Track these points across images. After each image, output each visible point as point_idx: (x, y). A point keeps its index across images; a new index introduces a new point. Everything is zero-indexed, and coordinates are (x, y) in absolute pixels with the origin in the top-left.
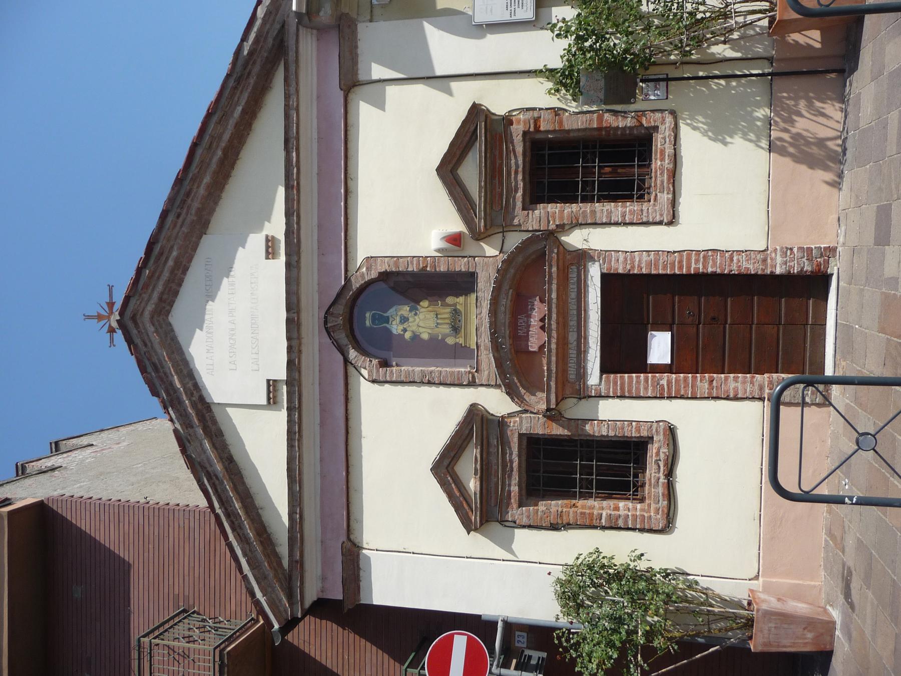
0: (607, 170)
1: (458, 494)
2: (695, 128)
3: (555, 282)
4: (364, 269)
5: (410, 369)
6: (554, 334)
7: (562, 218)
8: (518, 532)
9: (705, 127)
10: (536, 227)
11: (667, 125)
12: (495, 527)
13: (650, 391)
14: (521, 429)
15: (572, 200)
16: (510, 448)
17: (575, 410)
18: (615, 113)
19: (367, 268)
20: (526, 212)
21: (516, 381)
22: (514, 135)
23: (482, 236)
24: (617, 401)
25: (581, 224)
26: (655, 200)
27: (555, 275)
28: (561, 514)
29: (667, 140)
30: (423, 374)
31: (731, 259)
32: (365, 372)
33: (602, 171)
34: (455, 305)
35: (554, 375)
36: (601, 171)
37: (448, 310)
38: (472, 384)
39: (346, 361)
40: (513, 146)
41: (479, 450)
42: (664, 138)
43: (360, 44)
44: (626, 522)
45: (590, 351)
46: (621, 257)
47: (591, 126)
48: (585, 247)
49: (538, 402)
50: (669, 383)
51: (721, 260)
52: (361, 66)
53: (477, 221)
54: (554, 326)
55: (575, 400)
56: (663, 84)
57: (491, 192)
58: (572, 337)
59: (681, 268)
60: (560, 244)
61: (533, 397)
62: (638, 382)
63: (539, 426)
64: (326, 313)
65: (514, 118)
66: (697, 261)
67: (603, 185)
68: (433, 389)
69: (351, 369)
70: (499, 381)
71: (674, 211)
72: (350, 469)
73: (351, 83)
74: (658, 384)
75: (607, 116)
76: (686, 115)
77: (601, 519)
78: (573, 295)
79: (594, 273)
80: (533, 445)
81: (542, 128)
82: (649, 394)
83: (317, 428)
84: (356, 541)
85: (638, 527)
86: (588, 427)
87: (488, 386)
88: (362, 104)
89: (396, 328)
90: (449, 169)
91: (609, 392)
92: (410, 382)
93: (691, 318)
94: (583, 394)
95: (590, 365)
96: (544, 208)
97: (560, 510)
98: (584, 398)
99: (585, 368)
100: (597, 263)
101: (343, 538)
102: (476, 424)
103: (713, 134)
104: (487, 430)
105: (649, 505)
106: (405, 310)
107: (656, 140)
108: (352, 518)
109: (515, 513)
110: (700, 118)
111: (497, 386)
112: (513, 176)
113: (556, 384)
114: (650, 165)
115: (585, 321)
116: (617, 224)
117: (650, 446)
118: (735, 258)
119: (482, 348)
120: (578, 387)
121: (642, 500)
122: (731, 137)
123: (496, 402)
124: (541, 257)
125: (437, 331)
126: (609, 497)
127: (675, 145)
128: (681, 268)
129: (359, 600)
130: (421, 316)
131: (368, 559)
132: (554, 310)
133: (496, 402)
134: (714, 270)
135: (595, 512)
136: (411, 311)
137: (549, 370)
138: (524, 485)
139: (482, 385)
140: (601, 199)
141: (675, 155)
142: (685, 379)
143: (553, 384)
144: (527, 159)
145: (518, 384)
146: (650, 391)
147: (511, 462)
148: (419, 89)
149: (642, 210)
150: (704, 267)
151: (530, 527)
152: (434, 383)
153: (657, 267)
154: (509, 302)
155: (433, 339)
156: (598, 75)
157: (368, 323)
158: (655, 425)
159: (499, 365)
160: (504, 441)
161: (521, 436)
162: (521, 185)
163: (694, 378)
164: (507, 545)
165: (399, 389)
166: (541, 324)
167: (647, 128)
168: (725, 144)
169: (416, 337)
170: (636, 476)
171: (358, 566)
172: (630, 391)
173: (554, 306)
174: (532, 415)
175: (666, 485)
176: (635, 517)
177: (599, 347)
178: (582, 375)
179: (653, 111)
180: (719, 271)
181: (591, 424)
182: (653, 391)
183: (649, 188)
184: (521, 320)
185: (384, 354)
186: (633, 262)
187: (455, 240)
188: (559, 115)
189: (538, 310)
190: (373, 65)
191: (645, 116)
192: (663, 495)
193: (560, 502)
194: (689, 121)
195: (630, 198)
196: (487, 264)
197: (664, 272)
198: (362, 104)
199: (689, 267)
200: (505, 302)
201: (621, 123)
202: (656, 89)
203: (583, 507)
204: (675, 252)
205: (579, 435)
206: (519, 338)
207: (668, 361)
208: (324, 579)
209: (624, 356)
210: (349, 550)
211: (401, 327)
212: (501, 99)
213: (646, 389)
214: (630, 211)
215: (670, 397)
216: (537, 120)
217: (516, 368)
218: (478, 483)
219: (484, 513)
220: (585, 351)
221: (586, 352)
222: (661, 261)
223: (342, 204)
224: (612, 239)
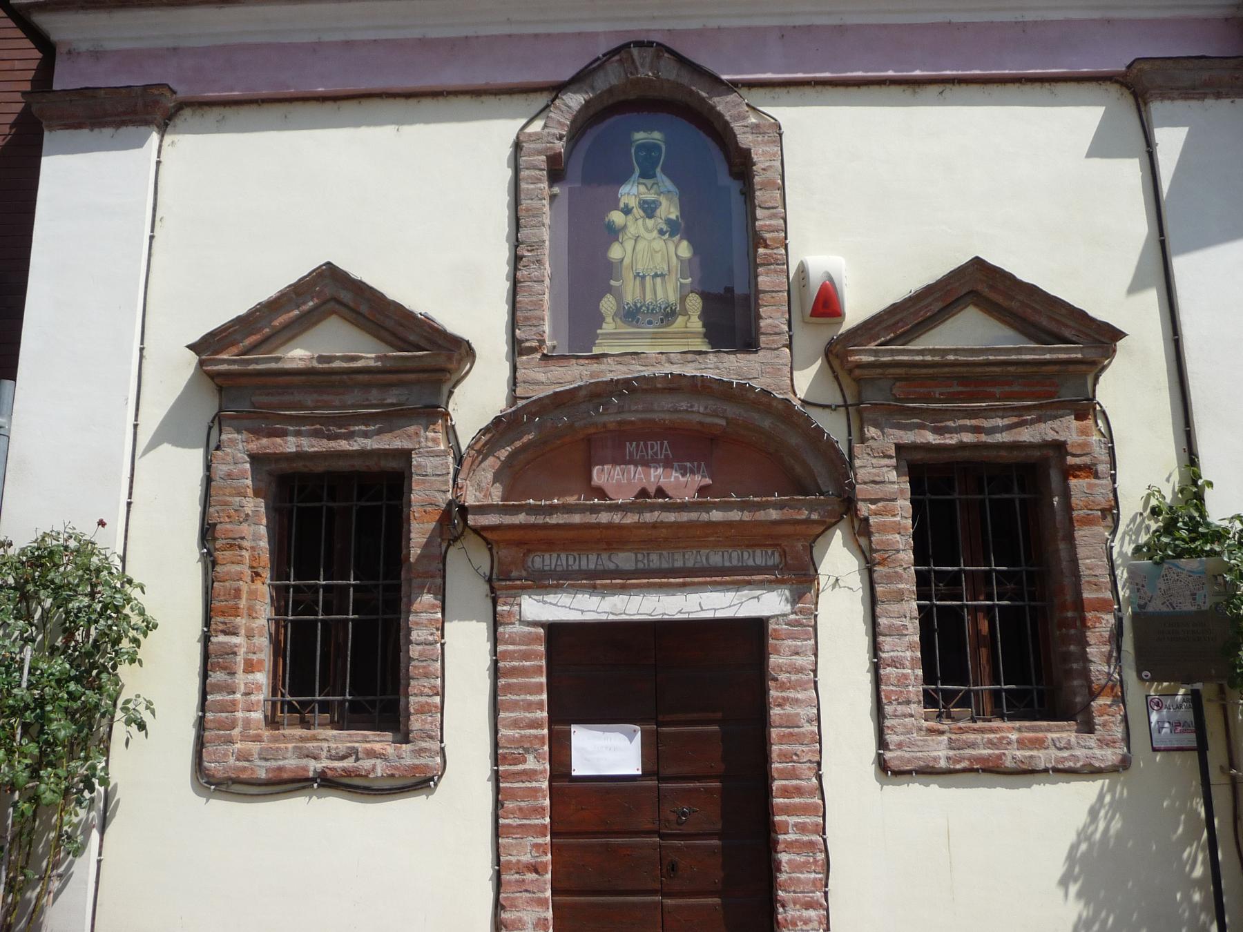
0: (984, 626)
1: (276, 323)
2: (1093, 813)
3: (747, 516)
4: (753, 120)
5: (547, 221)
6: (631, 519)
7: (884, 529)
8: (196, 457)
9: (1098, 836)
10: (862, 474)
11: (1098, 752)
12: (208, 406)
13: (510, 732)
14: (421, 455)
15: (920, 556)
16: (379, 432)
17: (466, 570)
18: (1117, 635)
19: (757, 126)
20: (892, 452)
21: (525, 439)
22: (1056, 424)
23: (836, 363)
24: (486, 661)
25: (870, 572)
26: (931, 731)
27: (761, 515)
28: (235, 545)
29: (1065, 754)
30: (535, 246)
31: (809, 905)
32: (537, 126)
33: (980, 615)
34: (685, 312)
35: (540, 520)
36: (979, 611)
37: (673, 297)
38: (517, 348)
39: (558, 89)
40: (1032, 422)
41: (372, 363)
42: (1068, 747)
43: (1225, 103)
44: (219, 688)
45: (595, 600)
46: (804, 661)
47: (1084, 586)
48: (823, 580)
49: (480, 488)
50: (530, 775)
51: (807, 882)
52: (1180, 106)
53: (872, 346)
54: (649, 517)
55: (486, 569)
56: (1190, 739)
57: (933, 378)
58: (624, 559)
59: (786, 792)
60: (827, 527)
61: (490, 476)
62: (529, 706)
63: (427, 494)
64: (658, 44)
65: (1090, 422)
66: (802, 828)
67: (952, 618)
68: (504, 269)
69: (541, 100)
70: (521, 403)
71: (909, 772)
72: (329, 106)
73: (1141, 88)
74: (527, 750)
75: (1109, 619)
76: (1122, 791)
77: (225, 633)
78: (716, 559)
79: (767, 603)
80: (387, 484)
81: (1073, 482)
82: (503, 732)
83: (416, 33)
84: (178, 121)
85: (209, 715)
86: (427, 599)
87: (514, 382)
88: (1099, 111)
89: (631, 193)
90: (978, 285)
91: (506, 643)
92: (517, 220)
93: (673, 817)
94: (500, 585)
95: (564, 599)
96: (902, 491)
97: (245, 544)
98: (492, 589)
99: (557, 588)
100: (788, 608)
101: (183, 92)
102: (429, 357)
103: (1083, 854)
104: (418, 382)
105: (257, 739)
106: (669, 210)
107: (1062, 730)
108: (227, 111)
109: (239, 448)
110: (1116, 825)
111: (513, 398)
112: (968, 422)
113: (521, 527)
114: (1002, 717)
115: (661, 586)
116: (875, 648)
117: (389, 735)
118: (812, 913)
119: (595, 367)
120: (514, 574)
121: (272, 722)
122: (1079, 895)
123: (478, 399)
124: (800, 486)
125: (628, 276)
126: (278, 651)
127: (1056, 770)
128: (786, 792)
129: (51, 128)
130: (658, 244)
131: (140, 143)
132: (685, 517)
133: (478, 399)
134: (785, 867)
135: (241, 621)
136: (669, 222)
137: (553, 509)
138: (299, 466)
139: (514, 369)
140: (925, 615)
141: (1033, 772)
142: (538, 811)
143: (521, 518)
144: (1003, 453)
145: (518, 444)
146: (510, 732)
147: (349, 436)
148: (1139, 227)
149: (908, 702)
150: (790, 845)
151: (208, 480)
152: (516, 269)
153: (784, 739)
154: (698, 418)
155: (611, 269)
156: (1206, 601)
157: (640, 136)
158: (435, 746)
159: (560, 401)
160: (392, 418)
161: (406, 455)
162: (951, 440)
163: (540, 830)
164: (170, 432)
165: (502, 199)
166: (652, 490)
167: (1087, 708)
168: (1064, 882)
169: (614, 233)
170: (325, 707)
171: (123, 123)
172: (509, 688)
173: (693, 516)
174: (451, 476)
175: (301, 774)
176: (231, 707)
177: (604, 617)
178: (542, 583)
179: (1125, 719)
180: (782, 877)
181: (434, 606)
182: (511, 740)
183: (949, 716)
184: (659, 448)
185: (575, 169)
186: (793, 686)
187: (827, 304)
188: (1104, 517)
189: (682, 483)
190: (1186, 129)
191: (1114, 703)
192: (280, 769)
193: (264, 544)
194: (1108, 799)
195: (929, 678)
196: (777, 372)
197: (774, 756)
198: (1099, 111)
199: (788, 810)
200: (698, 411)
201: (1096, 651)
202: (1175, 726)
203: (253, 595)
204: (819, 778)
205: (410, 581)
206: (621, 443)
207: (578, 769)
208: (97, 55)
209: (589, 673)
210: (156, 102)
211: (633, 202)
212: (1129, 393)
213: (516, 724)
214: (906, 677)
215: (497, 777)
216: (1090, 470)
217: (552, 436)
218: (301, 365)
219: (237, 377)
220: (594, 587)
221: (593, 589)
222: (798, 748)
223: (891, 73)
224: (840, 643)
